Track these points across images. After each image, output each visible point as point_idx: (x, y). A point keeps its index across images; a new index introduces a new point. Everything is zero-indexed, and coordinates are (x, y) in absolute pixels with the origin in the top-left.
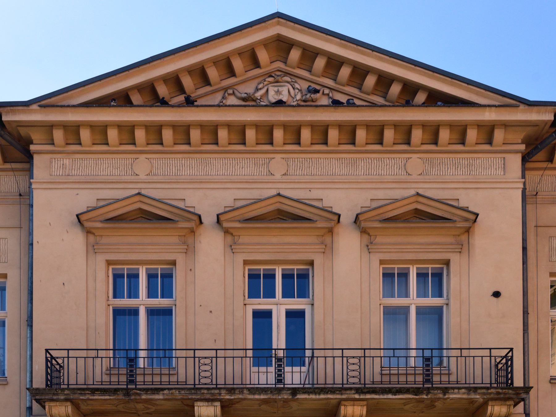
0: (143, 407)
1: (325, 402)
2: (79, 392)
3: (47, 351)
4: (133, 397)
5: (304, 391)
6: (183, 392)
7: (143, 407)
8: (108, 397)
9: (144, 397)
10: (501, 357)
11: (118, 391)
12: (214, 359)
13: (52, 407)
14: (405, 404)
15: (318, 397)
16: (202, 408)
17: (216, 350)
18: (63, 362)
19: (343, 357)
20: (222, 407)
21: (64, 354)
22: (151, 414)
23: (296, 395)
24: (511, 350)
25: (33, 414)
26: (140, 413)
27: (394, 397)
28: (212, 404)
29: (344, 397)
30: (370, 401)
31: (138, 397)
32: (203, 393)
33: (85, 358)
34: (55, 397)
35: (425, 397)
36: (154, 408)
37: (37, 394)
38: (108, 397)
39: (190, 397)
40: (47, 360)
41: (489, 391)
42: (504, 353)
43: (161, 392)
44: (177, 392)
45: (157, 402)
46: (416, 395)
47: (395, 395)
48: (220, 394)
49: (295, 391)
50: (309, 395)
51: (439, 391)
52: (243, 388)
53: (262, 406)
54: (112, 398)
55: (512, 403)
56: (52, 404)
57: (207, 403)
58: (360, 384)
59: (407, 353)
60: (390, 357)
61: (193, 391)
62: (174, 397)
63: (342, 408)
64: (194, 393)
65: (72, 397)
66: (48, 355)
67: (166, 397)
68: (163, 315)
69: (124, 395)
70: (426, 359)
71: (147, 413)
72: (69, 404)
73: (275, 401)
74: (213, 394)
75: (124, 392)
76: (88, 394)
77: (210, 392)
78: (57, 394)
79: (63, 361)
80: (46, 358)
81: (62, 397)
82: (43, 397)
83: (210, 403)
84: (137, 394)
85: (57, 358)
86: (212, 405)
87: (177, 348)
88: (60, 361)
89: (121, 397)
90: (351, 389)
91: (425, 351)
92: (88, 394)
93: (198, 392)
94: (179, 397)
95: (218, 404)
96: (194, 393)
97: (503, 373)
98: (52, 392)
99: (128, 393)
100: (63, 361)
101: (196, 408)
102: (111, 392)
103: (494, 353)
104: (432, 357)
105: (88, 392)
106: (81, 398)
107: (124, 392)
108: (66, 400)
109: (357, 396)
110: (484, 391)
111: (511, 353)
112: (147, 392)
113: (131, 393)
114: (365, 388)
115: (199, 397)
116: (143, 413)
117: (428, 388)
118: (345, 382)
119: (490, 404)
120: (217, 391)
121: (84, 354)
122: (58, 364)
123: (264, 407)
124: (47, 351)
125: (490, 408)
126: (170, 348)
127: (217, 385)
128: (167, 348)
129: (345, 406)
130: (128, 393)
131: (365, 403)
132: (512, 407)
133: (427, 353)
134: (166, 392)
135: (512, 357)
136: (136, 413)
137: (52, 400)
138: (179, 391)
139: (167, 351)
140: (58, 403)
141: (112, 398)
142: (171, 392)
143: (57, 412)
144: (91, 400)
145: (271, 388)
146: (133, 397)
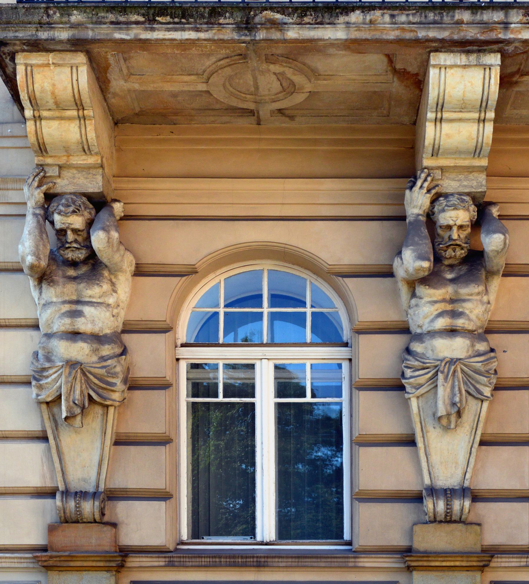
2: (111, 17)
4: (261, 35)
6: (403, 18)
8: (192, 35)
9: (292, 34)
11: (220, 15)
13: (35, 70)
16: (450, 71)
22: (292, 118)
28: (478, 58)
31: (276, 35)
32: (460, 22)
34: (43, 35)
38: (192, 35)
39: (421, 34)
43: (342, 19)
44: (387, 18)
48: (506, 25)
52: (198, 7)
54: (202, 35)
56: (36, 59)
57: (464, 57)
61: (431, 16)
62: (377, 35)
64: (435, 22)
65: (90, 34)
67: (355, 34)
68: (252, 322)
69: (239, 28)
74: (486, 26)
75: (239, 16)
76: (137, 23)
77: (478, 17)
78: (50, 26)
81: (64, 35)
82: (10, 35)
83: (473, 58)
84: (274, 24)
86: (478, 65)
89: (229, 33)
92: (137, 23)
93: (446, 19)
94: (392, 35)
95: (494, 60)
96: (435, 22)
98: (36, 19)
99: (247, 23)
101: (433, 73)
102: (202, 16)
105: (135, 17)
106: (118, 35)
107: (239, 16)
108: (77, 45)
112: (301, 17)
113: (257, 19)
115: (445, 34)
120: (498, 16)
130: (247, 23)
134: (356, 17)
136: (252, 112)
137: (35, 46)
138: (392, 16)
140: (51, 58)
141: (202, 35)
142: (368, 18)
143: (47, 86)
146: (261, 35)
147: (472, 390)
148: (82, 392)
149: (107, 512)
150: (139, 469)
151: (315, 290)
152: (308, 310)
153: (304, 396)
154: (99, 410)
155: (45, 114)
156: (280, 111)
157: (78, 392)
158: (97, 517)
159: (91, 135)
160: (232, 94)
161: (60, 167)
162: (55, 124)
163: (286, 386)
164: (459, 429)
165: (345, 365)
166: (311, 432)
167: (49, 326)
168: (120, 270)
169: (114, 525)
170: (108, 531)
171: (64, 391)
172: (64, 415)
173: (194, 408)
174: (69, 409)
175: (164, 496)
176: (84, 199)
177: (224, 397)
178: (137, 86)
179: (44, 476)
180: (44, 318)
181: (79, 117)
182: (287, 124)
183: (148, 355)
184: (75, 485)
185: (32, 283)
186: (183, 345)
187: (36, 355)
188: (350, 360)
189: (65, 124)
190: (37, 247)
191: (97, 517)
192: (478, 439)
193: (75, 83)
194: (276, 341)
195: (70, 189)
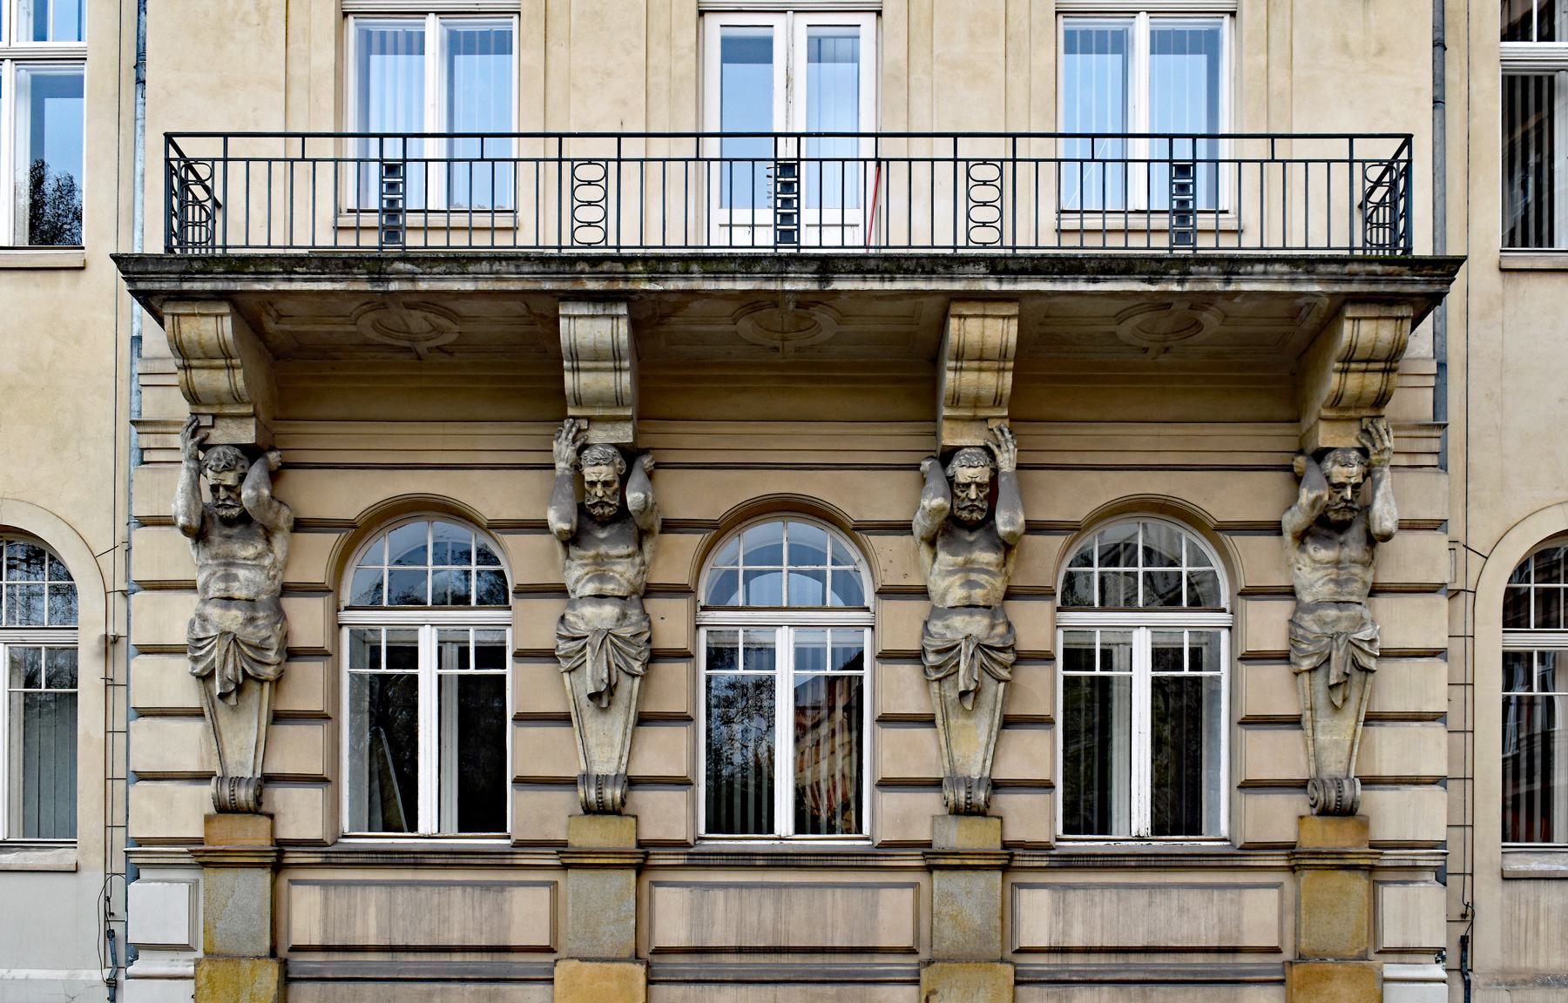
0: (426, 327)
1: (903, 306)
3: (169, 138)
5: (858, 265)
7: (426, 327)
10: (1380, 162)
12: (613, 166)
14: (1120, 318)
15: (887, 286)
17: (1351, 137)
18: (212, 175)
19: (1351, 161)
20: (635, 325)
21: (213, 148)
22: (451, 353)
23: (829, 281)
24: (1408, 139)
25: (144, 353)
26: (422, 347)
27: (1092, 287)
29: (958, 286)
30: (1031, 304)
33: (642, 160)
35: (1175, 287)
36: (456, 328)
37: (144, 275)
40: (170, 171)
41: (1348, 268)
42: (1387, 149)
45: (463, 307)
46: (1151, 282)
47: (1095, 281)
49: (826, 265)
50: (1000, 281)
51: (1213, 269)
53: (741, 322)
55: (1406, 311)
58: (1002, 247)
59: (1125, 149)
60: (471, 161)
63: (954, 323)
66: (173, 154)
68: (1191, 52)
70: (1178, 167)
71: (440, 348)
72: (225, 308)
73: (775, 298)
79: (212, 170)
80: (168, 160)
85: (197, 161)
87: (456, 131)
88: (203, 171)
90: (976, 260)
91: (386, 140)
97: (1384, 215)
100: (212, 170)
101: (563, 323)
103: (1363, 149)
104: (405, 160)
109: (993, 286)
110: (1333, 268)
111: (1406, 149)
114: (1015, 258)
116: (430, 350)
117: (1185, 260)
118: (961, 242)
119: (1349, 314)
121: (275, 147)
122: (200, 181)
123: (745, 326)
124: (169, 138)
125: (1347, 327)
126: (1212, 132)
127: (225, 247)
128: (803, 130)
129: (960, 317)
131: (1013, 309)
132: (1408, 324)
133: (1183, 150)
135: (1409, 162)
136: (409, 350)
139: (803, 139)
144: (708, 294)
145: (945, 257)
147: (622, 664)
148: (235, 666)
149: (264, 800)
150: (299, 750)
151: (1193, 547)
152: (829, 568)
153: (1182, 669)
154: (256, 686)
155: (194, 363)
156: (438, 348)
157: (230, 666)
158: (251, 804)
159: (240, 383)
160: (383, 334)
161: (215, 417)
162: (205, 373)
163: (1164, 657)
164: (614, 709)
165: (1225, 634)
166: (480, 712)
167: (943, 597)
168: (277, 528)
169: (272, 816)
170: (265, 823)
171: (217, 665)
172: (218, 691)
173: (1157, 684)
174: (223, 684)
175: (684, 783)
176: (237, 452)
177: (477, 667)
178: (288, 327)
179: (202, 760)
180: (937, 585)
181: (1383, 371)
182: (446, 359)
183: (308, 621)
184: (233, 772)
185: (559, 547)
186: (347, 609)
187: (192, 623)
188: (1230, 628)
189: (215, 373)
190: (188, 506)
191: (251, 804)
192: (1362, 718)
193: (614, 333)
194: (752, 604)
195: (224, 440)
